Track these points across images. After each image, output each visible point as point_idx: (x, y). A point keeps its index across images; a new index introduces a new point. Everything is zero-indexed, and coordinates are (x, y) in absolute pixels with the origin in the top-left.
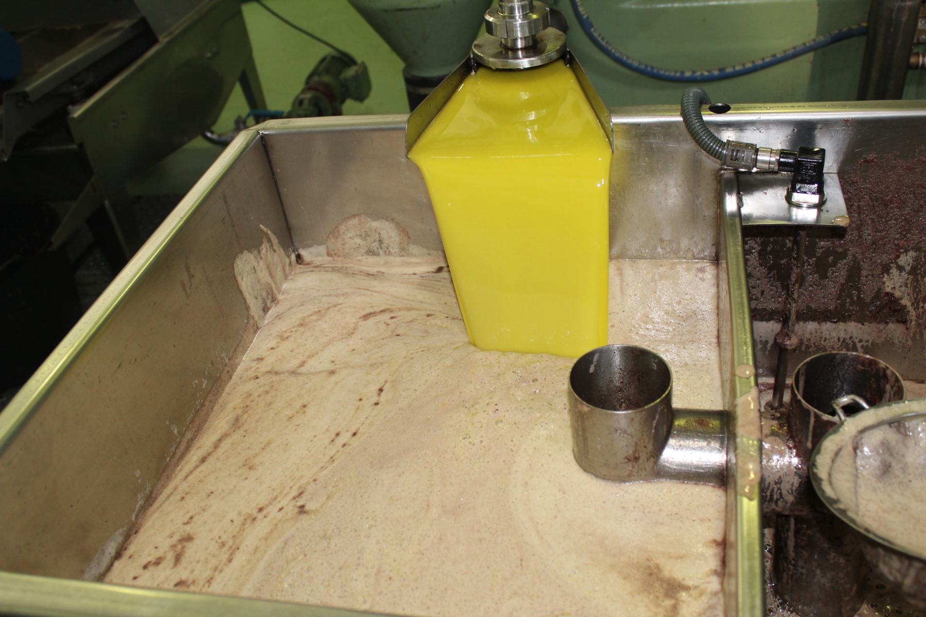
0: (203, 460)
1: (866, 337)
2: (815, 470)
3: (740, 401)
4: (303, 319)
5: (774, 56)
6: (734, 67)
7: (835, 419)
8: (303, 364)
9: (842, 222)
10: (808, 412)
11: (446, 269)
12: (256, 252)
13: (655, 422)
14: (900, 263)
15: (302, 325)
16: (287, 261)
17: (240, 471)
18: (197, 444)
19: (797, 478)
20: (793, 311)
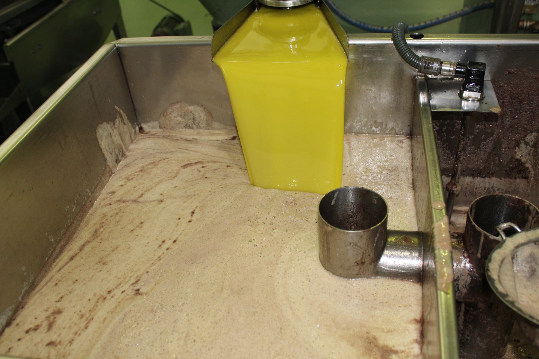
0: (72, 259)
1: (502, 187)
2: (489, 273)
3: (436, 225)
4: (143, 167)
5: (438, 19)
6: (413, 25)
7: (499, 238)
8: (142, 195)
9: (496, 110)
10: (480, 233)
11: (237, 138)
12: (112, 124)
13: (376, 238)
14: (527, 140)
15: (142, 171)
16: (133, 131)
17: (96, 266)
18: (68, 248)
19: (469, 277)
20: (459, 169)
